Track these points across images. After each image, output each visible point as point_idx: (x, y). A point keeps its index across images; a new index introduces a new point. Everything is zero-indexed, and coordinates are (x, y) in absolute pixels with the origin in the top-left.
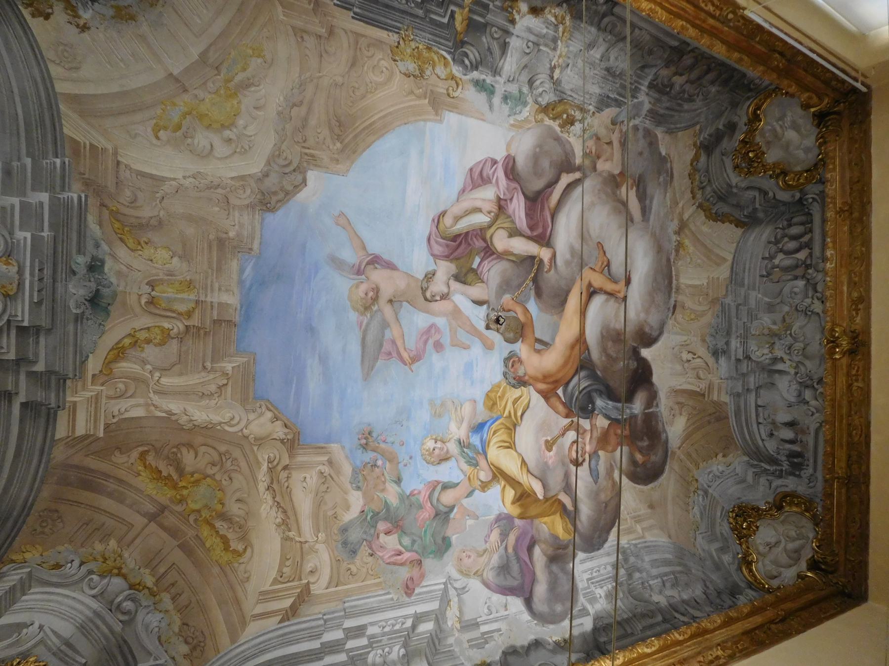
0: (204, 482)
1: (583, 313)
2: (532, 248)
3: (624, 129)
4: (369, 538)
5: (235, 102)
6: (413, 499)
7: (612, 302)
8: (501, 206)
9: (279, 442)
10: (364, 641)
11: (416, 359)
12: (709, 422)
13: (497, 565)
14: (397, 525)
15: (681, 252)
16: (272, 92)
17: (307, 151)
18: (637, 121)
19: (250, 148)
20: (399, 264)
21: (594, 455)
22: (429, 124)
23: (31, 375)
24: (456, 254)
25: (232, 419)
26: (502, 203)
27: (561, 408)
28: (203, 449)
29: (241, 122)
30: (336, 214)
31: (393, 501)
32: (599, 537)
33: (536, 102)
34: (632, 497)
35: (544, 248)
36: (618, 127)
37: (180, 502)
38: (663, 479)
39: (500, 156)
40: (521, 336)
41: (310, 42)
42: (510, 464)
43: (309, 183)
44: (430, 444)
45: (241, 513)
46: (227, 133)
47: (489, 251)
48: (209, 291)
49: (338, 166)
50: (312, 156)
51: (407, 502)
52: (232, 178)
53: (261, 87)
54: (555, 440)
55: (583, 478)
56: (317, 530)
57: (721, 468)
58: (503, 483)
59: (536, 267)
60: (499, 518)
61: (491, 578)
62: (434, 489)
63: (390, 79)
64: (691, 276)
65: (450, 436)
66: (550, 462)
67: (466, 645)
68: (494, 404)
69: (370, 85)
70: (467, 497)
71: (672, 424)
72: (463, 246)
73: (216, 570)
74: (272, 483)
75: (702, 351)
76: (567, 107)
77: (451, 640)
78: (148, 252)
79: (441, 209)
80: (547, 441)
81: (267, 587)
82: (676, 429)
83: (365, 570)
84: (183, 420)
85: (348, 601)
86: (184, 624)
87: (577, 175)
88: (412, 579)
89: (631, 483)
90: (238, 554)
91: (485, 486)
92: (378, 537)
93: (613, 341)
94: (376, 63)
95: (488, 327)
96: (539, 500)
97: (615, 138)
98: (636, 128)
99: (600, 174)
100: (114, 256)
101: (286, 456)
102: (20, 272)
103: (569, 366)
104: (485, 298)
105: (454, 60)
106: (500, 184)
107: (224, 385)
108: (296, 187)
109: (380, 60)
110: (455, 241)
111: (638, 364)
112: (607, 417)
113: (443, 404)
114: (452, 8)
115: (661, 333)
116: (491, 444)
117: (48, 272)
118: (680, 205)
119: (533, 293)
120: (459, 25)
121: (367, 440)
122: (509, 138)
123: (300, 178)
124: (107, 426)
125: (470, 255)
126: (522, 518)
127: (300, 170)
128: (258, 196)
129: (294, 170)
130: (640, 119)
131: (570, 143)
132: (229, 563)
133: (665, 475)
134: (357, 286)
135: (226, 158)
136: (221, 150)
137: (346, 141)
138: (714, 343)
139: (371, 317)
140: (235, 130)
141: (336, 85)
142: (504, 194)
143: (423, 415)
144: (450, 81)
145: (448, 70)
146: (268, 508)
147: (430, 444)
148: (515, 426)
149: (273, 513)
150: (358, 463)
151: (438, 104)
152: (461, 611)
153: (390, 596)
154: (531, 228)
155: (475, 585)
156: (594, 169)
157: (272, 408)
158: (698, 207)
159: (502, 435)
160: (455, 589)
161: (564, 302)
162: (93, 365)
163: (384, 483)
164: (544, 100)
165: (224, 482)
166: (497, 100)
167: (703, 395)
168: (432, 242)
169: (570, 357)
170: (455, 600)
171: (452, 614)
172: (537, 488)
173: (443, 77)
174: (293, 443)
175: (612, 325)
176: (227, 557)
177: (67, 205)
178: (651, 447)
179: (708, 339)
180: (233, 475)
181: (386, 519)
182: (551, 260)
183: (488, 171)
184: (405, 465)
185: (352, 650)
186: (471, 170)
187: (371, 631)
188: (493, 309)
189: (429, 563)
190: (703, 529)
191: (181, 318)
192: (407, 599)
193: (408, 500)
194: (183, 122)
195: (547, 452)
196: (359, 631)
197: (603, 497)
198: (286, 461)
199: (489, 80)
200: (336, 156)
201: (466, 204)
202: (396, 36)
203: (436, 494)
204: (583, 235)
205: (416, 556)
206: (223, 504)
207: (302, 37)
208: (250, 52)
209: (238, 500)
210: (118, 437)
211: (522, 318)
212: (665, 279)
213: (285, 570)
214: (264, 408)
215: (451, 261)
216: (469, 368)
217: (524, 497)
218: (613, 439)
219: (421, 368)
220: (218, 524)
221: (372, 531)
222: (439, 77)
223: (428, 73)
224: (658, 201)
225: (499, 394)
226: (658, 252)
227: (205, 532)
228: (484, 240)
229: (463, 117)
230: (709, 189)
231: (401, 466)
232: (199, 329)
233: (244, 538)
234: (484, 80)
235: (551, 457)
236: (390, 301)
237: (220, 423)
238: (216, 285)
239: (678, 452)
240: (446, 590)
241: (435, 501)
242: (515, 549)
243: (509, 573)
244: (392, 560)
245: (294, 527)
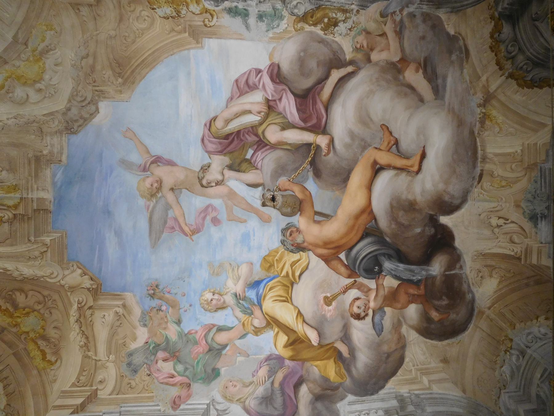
0: (32, 314)
1: (369, 187)
2: (308, 137)
3: (398, 18)
4: (149, 362)
5: (41, 64)
6: (190, 337)
7: (403, 175)
8: (270, 107)
9: (86, 290)
11: (196, 231)
12: (527, 285)
13: (260, 396)
14: (174, 355)
15: (488, 123)
16: (67, 53)
17: (97, 88)
18: (412, 9)
19: (55, 93)
20: (178, 161)
21: (379, 310)
22: (192, 52)
24: (229, 149)
25: (52, 274)
26: (271, 103)
27: (343, 270)
28: (31, 293)
29: (47, 77)
30: (124, 130)
32: (375, 384)
33: (292, 14)
34: (419, 351)
35: (320, 136)
36: (389, 17)
37: (16, 326)
38: (465, 336)
39: (264, 64)
40: (299, 210)
41: (85, 11)
42: (285, 314)
43: (100, 110)
45: (56, 336)
46: (38, 86)
47: (262, 144)
48: (30, 191)
49: (122, 95)
50: (101, 91)
51: (184, 339)
52: (44, 115)
53: (57, 50)
54: (334, 297)
55: (361, 332)
56: (109, 353)
57: (543, 330)
58: (276, 330)
59: (313, 152)
60: (269, 358)
61: (252, 406)
62: (210, 331)
63: (152, 24)
64: (502, 144)
65: (228, 290)
66: (328, 315)
68: (271, 266)
69: (137, 32)
70: (240, 339)
71: (480, 285)
72: (235, 142)
73: (35, 372)
74: (80, 317)
75: (515, 216)
76: (327, 11)
79: (212, 115)
80: (326, 298)
81: (67, 388)
82: (485, 290)
83: (141, 386)
84: (16, 274)
85: (124, 407)
86: (8, 405)
87: (350, 69)
88: (180, 397)
89: (422, 338)
90: (51, 363)
91: (257, 331)
92: (157, 363)
93: (405, 211)
94: (138, 15)
95: (264, 205)
96: (313, 346)
97: (389, 29)
98: (412, 16)
99: (376, 64)
101: (91, 299)
103: (354, 232)
104: (261, 181)
106: (267, 88)
107: (45, 252)
108: (91, 115)
109: (141, 11)
110: (227, 139)
111: (436, 231)
112: (397, 277)
113: (221, 266)
115: (464, 200)
116: (267, 297)
118: (484, 78)
119: (311, 174)
121: (154, 291)
122: (270, 50)
123: (93, 108)
125: (244, 148)
126: (293, 360)
127: (94, 102)
128: (64, 125)
129: (89, 103)
130: (416, 5)
131: (336, 42)
132: (44, 369)
133: (467, 333)
134: (144, 180)
135: (39, 102)
136: (34, 96)
137: (126, 76)
138: (531, 208)
139: (157, 202)
140: (43, 83)
141: (111, 37)
142: (272, 96)
143: (203, 274)
144: (204, 14)
145: (201, 6)
146: (76, 334)
147: (208, 296)
148: (292, 284)
149: (79, 338)
150: (147, 308)
151: (197, 35)
153: (159, 408)
154: (304, 120)
156: (369, 60)
157: (82, 267)
158: (507, 78)
159: (279, 291)
160: (217, 410)
161: (346, 180)
163: (167, 323)
164: (301, 11)
165: (46, 315)
166: (252, 20)
167: (519, 259)
168: (206, 141)
169: (354, 226)
172: (313, 336)
173: (198, 12)
174: (96, 291)
175: (404, 197)
176: (42, 365)
178: (451, 307)
179: (523, 205)
180: (53, 311)
181: (165, 350)
182: (329, 146)
183: (253, 79)
184: (186, 311)
186: (237, 81)
188: (269, 190)
189: (196, 387)
190: (512, 387)
191: (10, 209)
192: (173, 412)
193: (187, 338)
194: (6, 84)
195: (325, 306)
197: (385, 348)
198: (91, 303)
199: (241, 5)
200: (120, 88)
201: (235, 108)
203: (211, 334)
204: (364, 118)
205: (187, 381)
206: (44, 330)
207: (78, 9)
208: (45, 28)
209: (55, 328)
211: (300, 195)
212: (468, 151)
213: (82, 378)
214: (75, 267)
215: (225, 155)
216: (246, 238)
217: (296, 342)
218: (403, 298)
219: (201, 238)
220: (40, 342)
221: (153, 358)
222: (194, 13)
223: (183, 12)
224: (452, 80)
225: (276, 258)
226: (459, 126)
227: (31, 346)
228: (257, 135)
229: (223, 41)
230: (521, 58)
231: (182, 311)
232: (23, 216)
233: (57, 352)
234: (236, 7)
235: (330, 311)
236: (172, 189)
237: (43, 277)
238: (35, 186)
239: (488, 312)
241: (209, 340)
242: (282, 384)
243: (271, 404)
244: (165, 381)
245: (92, 349)
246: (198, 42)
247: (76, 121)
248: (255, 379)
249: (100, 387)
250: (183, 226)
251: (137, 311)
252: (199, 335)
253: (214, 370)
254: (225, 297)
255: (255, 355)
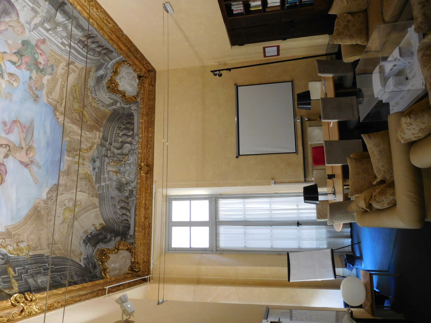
10: (63, 40)
11: (15, 122)
14: (37, 63)
23: (106, 147)
29: (62, 211)
31: (34, 71)
43: (46, 194)
44: (15, 84)
56: (58, 79)
62: (19, 66)
67: (41, 8)
70: (7, 53)
77: (44, 14)
78: (84, 173)
81: (73, 73)
88: (41, 43)
90: (74, 86)
100: (90, 171)
102: (107, 168)
105: (7, 255)
114: (17, 275)
117: (102, 168)
120: (10, 270)
121: (36, 98)
124: (93, 132)
127: (48, 198)
134: (33, 156)
145: (7, 250)
147: (15, 84)
152: (34, 18)
155: (22, 20)
162: (95, 146)
168: (5, 172)
170: (33, 23)
171: (38, 20)
174: (55, 109)
177: (98, 183)
181: (39, 68)
185: (67, 41)
187: (60, 41)
189: (34, 43)
193: (29, 69)
196: (63, 44)
198: (58, 104)
202: (30, 254)
210: (91, 128)
221: (44, 68)
223: (15, 245)
227: (78, 96)
231: (28, 83)
240: (34, 29)
246: (7, 229)
247: (54, 190)
248: (7, 27)
249: (64, 67)
250: (20, 127)
251: (44, 92)
252: (24, 66)
253: (24, 45)
254: (8, 80)
255: (2, 39)
